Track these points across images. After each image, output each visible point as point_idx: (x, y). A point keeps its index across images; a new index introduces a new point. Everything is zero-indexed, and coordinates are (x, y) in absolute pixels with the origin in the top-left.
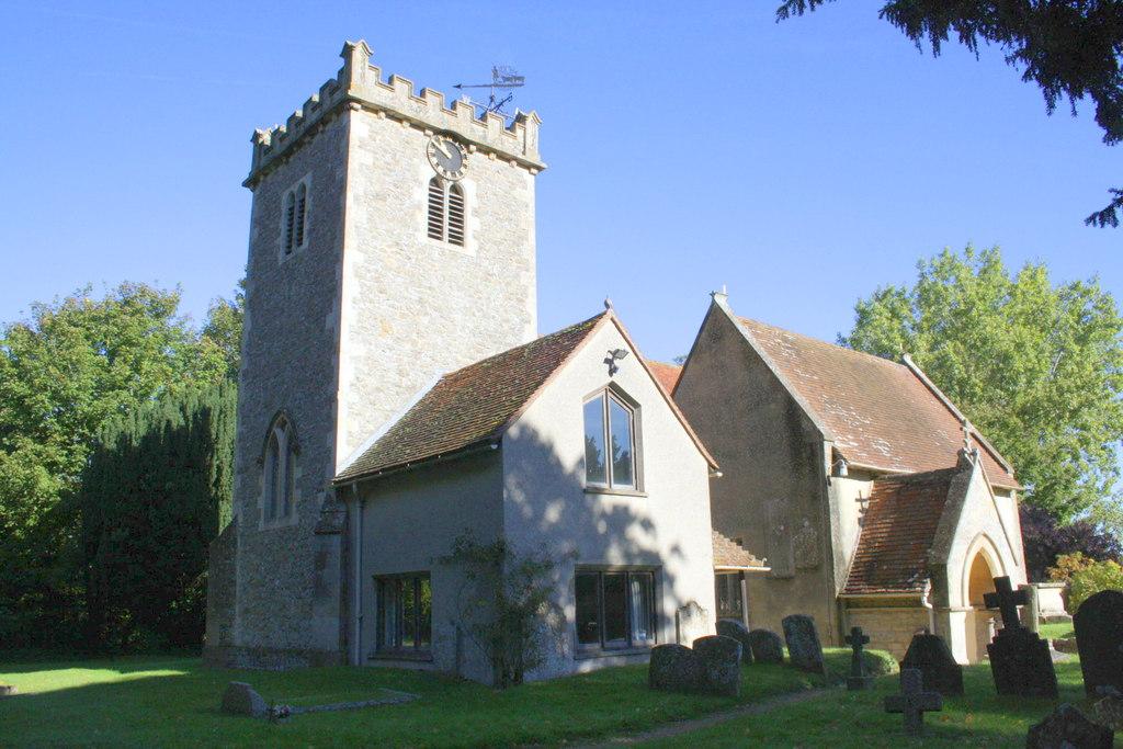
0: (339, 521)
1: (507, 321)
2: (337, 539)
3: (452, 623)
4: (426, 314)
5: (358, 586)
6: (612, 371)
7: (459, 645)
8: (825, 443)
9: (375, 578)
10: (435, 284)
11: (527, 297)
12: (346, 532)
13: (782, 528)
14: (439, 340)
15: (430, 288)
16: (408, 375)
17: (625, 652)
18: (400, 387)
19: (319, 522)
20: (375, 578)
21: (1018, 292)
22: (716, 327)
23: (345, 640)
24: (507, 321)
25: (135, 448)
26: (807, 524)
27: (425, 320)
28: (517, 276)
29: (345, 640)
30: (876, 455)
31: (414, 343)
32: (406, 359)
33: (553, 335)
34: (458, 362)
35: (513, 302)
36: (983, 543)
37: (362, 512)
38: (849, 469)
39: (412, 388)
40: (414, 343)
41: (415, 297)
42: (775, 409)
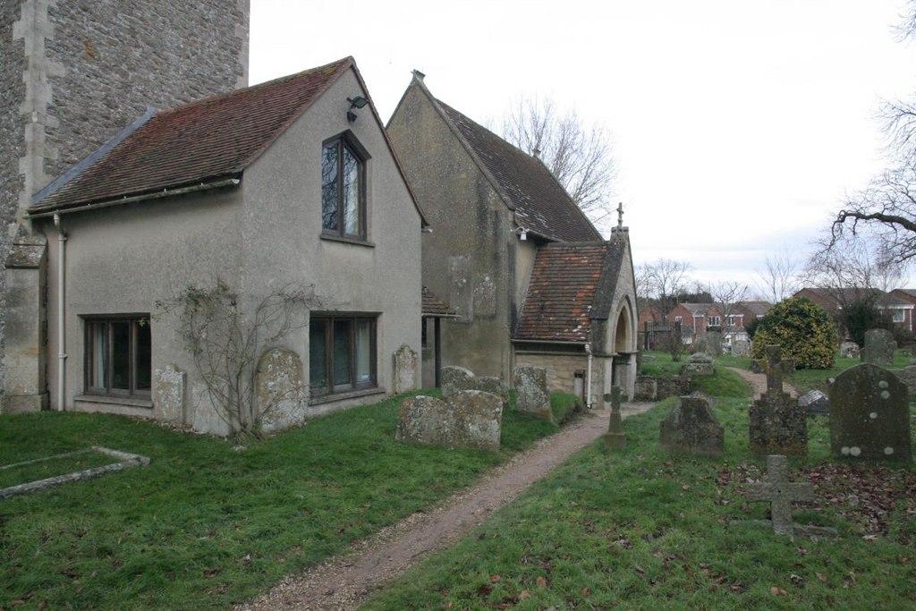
0: (36, 255)
1: (221, 70)
2: (32, 278)
3: (177, 370)
4: (137, 46)
5: (110, 342)
6: (351, 118)
7: (185, 397)
9: (81, 316)
10: (148, 15)
11: (240, 49)
12: (45, 266)
13: (465, 281)
14: (151, 76)
15: (142, 19)
16: (117, 107)
18: (108, 118)
19: (11, 256)
20: (81, 316)
21: (281, 496)
22: (381, 313)
24: (221, 70)
26: (487, 278)
27: (137, 53)
28: (232, 27)
29: (45, 389)
30: (539, 225)
31: (124, 75)
32: (114, 90)
33: (248, 32)
34: (171, 103)
35: (227, 53)
36: (625, 304)
37: (65, 250)
38: (529, 235)
39: (122, 123)
40: (124, 75)
41: (124, 24)
42: (468, 169)
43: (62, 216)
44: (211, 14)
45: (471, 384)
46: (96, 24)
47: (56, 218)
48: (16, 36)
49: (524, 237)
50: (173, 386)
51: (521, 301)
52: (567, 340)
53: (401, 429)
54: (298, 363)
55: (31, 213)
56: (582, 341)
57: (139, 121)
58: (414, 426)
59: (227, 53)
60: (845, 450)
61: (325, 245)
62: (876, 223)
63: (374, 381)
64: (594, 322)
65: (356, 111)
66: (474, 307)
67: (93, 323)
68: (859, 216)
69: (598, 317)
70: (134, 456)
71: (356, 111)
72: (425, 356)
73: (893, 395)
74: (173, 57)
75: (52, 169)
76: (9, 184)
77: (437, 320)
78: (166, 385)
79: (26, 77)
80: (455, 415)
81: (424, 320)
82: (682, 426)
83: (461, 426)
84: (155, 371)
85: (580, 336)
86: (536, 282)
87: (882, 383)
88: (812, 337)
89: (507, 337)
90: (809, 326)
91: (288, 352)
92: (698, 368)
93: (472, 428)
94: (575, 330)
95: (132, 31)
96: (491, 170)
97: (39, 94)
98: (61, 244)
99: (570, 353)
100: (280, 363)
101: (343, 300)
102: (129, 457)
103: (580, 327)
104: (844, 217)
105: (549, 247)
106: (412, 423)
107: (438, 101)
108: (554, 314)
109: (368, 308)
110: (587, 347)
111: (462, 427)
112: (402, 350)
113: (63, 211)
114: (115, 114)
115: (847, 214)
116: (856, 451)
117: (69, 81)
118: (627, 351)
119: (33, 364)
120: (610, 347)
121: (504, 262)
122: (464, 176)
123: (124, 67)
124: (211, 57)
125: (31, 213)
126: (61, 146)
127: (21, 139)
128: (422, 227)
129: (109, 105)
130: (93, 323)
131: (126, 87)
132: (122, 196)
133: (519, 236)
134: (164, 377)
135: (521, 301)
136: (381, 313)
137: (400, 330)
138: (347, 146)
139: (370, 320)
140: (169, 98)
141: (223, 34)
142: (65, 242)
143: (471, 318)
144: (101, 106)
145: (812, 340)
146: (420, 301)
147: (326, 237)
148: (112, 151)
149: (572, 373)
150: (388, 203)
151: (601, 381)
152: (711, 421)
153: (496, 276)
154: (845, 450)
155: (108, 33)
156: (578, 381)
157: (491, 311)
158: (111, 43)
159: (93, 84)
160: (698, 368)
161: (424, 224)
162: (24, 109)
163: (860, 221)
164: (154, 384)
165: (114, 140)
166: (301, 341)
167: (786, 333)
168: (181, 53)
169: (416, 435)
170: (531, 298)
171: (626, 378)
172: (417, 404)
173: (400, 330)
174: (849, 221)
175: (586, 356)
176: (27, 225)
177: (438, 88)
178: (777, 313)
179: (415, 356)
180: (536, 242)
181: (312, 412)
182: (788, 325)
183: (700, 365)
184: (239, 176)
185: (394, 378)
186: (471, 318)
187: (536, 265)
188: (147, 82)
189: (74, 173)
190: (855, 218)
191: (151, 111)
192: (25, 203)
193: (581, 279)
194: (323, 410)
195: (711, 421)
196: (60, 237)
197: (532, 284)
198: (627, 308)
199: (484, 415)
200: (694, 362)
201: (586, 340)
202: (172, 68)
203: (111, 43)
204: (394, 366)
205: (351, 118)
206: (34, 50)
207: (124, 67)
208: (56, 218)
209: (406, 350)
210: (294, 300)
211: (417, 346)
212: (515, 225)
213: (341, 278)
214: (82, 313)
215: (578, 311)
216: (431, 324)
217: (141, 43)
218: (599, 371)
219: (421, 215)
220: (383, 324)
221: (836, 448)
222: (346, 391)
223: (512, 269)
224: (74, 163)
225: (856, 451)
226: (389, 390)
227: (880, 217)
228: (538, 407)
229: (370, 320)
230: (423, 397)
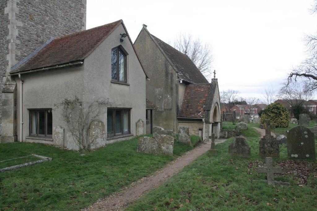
0: (12, 88)
1: (76, 24)
2: (11, 96)
3: (61, 128)
4: (47, 16)
6: (122, 41)
8: (306, 74)
9: (28, 109)
10: (51, 5)
11: (83, 17)
12: (15, 92)
13: (161, 97)
14: (52, 26)
15: (49, 7)
16: (40, 37)
17: (122, 136)
18: (37, 41)
19: (4, 88)
20: (28, 109)
23: (16, 134)
24: (76, 24)
25: (286, 139)
26: (169, 96)
27: (47, 18)
29: (16, 134)
30: (187, 78)
31: (43, 26)
32: (39, 31)
34: (59, 35)
35: (79, 18)
36: (216, 105)
37: (22, 86)
38: (183, 81)
39: (42, 43)
40: (43, 26)
41: (43, 8)
43: (21, 75)
44: (73, 5)
45: (163, 133)
46: (33, 8)
47: (19, 75)
48: (6, 12)
49: (181, 82)
51: (180, 104)
52: (196, 117)
53: (139, 148)
54: (103, 125)
55: (11, 73)
56: (201, 118)
57: (48, 42)
58: (143, 147)
59: (79, 18)
60: (292, 155)
61: (113, 85)
62: (303, 77)
63: (129, 132)
64: (205, 111)
65: (123, 38)
66: (164, 106)
67: (32, 112)
68: (297, 75)
69: (207, 109)
70: (46, 157)
71: (123, 38)
72: (147, 123)
73: (309, 136)
74: (60, 20)
75: (18, 58)
76: (3, 64)
77: (151, 110)
78: (58, 133)
79: (9, 27)
80: (157, 143)
81: (147, 111)
82: (236, 147)
83: (159, 147)
84: (54, 128)
85: (201, 116)
86: (185, 97)
87: (305, 132)
88: (281, 116)
89: (176, 116)
90: (280, 112)
91: (100, 122)
92: (242, 127)
93: (163, 148)
94: (199, 114)
95: (46, 11)
96: (170, 59)
97: (14, 32)
98: (21, 84)
99: (197, 122)
100: (97, 125)
101: (119, 104)
102: (45, 158)
103: (201, 113)
104: (292, 75)
105: (190, 85)
106: (143, 146)
107: (152, 35)
108: (192, 108)
109: (127, 106)
110: (203, 120)
111: (160, 148)
112: (139, 121)
113: (22, 73)
114: (40, 40)
115: (293, 74)
116: (296, 156)
117: (24, 28)
118: (217, 121)
119: (11, 126)
120: (211, 120)
121: (174, 90)
122: (160, 61)
123: (43, 23)
124: (73, 20)
125: (11, 73)
126: (21, 51)
127: (7, 48)
128: (146, 78)
129: (38, 36)
130: (32, 112)
131: (44, 30)
132: (42, 68)
133: (180, 81)
134: (57, 130)
135: (180, 104)
136: (132, 108)
137: (138, 114)
138: (120, 51)
139: (128, 110)
140: (58, 34)
141: (77, 12)
142: (23, 84)
143: (163, 110)
144: (35, 37)
145: (281, 118)
146: (145, 104)
147: (113, 82)
148: (39, 52)
149: (198, 129)
150: (134, 70)
151: (208, 132)
152: (246, 146)
153: (172, 95)
154: (292, 155)
155: (37, 11)
156: (200, 132)
157: (170, 107)
158: (39, 15)
159: (32, 29)
160: (242, 127)
161: (147, 77)
162: (8, 38)
163: (298, 76)
164: (53, 133)
165: (40, 48)
166: (104, 118)
167: (272, 115)
168: (63, 18)
169: (144, 150)
170: (184, 103)
171: (217, 131)
172: (144, 140)
173: (138, 114)
174: (294, 76)
175: (203, 123)
176: (9, 78)
177: (152, 30)
178: (269, 108)
179: (144, 123)
180: (186, 83)
181: (108, 142)
182: (273, 112)
183: (242, 126)
184: (83, 61)
185: (136, 131)
186: (163, 110)
187: (185, 91)
188: (51, 28)
189: (26, 60)
190: (296, 75)
191: (52, 38)
192: (9, 70)
193: (201, 97)
194: (112, 141)
196: (21, 82)
197: (184, 98)
198: (217, 106)
199: (168, 143)
200: (240, 125)
201: (203, 118)
202: (60, 24)
203: (39, 15)
204: (136, 126)
205: (122, 41)
206: (12, 17)
207: (43, 23)
208: (19, 75)
209: (141, 121)
210: (102, 104)
211: (144, 120)
212: (178, 78)
213: (118, 96)
214: (28, 108)
215: (200, 107)
216: (149, 112)
217: (49, 15)
218: (207, 128)
220: (133, 112)
221: (289, 155)
222: (120, 135)
223: (177, 93)
224: (25, 56)
225: (296, 156)
226: (135, 135)
227: (305, 75)
228: (186, 141)
229: (128, 110)
230: (146, 137)
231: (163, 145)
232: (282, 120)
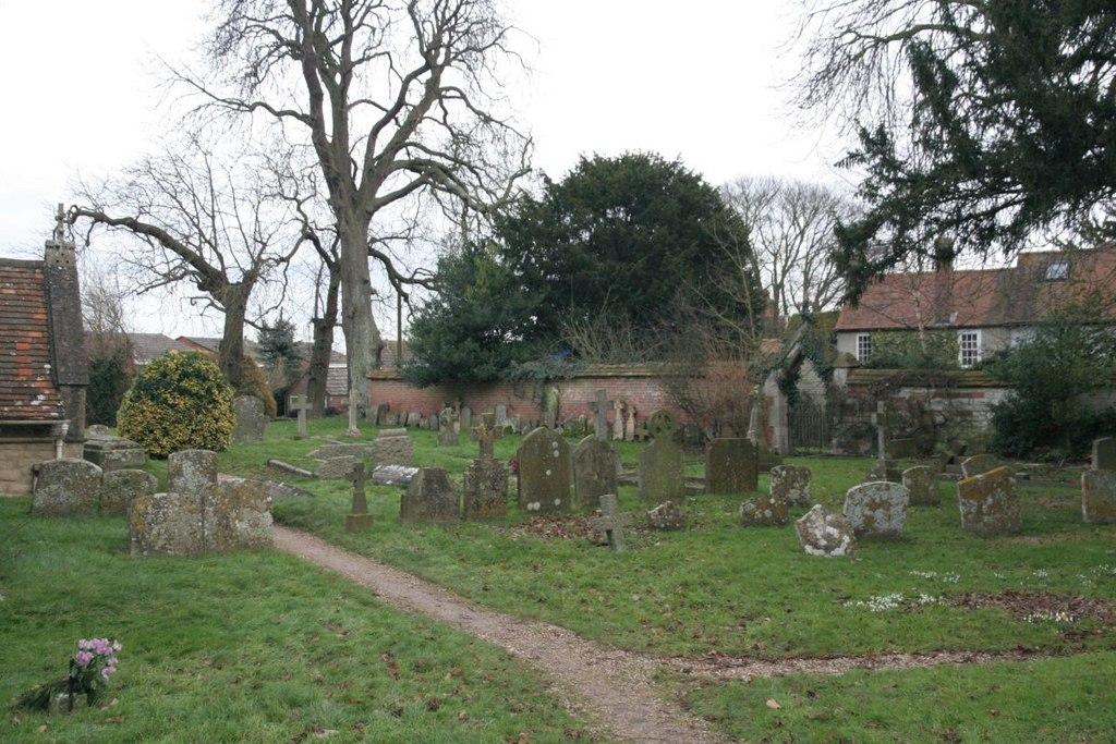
50: (951, 404)
52: (28, 418)
53: (138, 542)
56: (55, 418)
58: (159, 534)
60: (530, 506)
62: (125, 236)
64: (63, 389)
68: (99, 218)
69: (72, 382)
73: (561, 453)
80: (215, 512)
82: (425, 498)
83: (225, 525)
85: (48, 411)
88: (215, 408)
90: (209, 391)
92: (124, 455)
93: (240, 526)
94: (35, 403)
99: (21, 439)
104: (75, 216)
106: (154, 532)
111: (227, 526)
115: (80, 213)
116: (537, 506)
145: (216, 413)
149: (26, 470)
152: (450, 490)
160: (124, 455)
163: (101, 228)
167: (182, 403)
169: (163, 548)
172: (157, 505)
174: (83, 223)
178: (164, 375)
182: (183, 392)
190: (91, 219)
193: (15, 321)
195: (450, 490)
199: (254, 508)
200: (117, 448)
201: (62, 418)
215: (30, 372)
219: (1000, 326)
225: (537, 506)
227: (134, 226)
230: (165, 495)
231: (237, 518)
232: (217, 420)
